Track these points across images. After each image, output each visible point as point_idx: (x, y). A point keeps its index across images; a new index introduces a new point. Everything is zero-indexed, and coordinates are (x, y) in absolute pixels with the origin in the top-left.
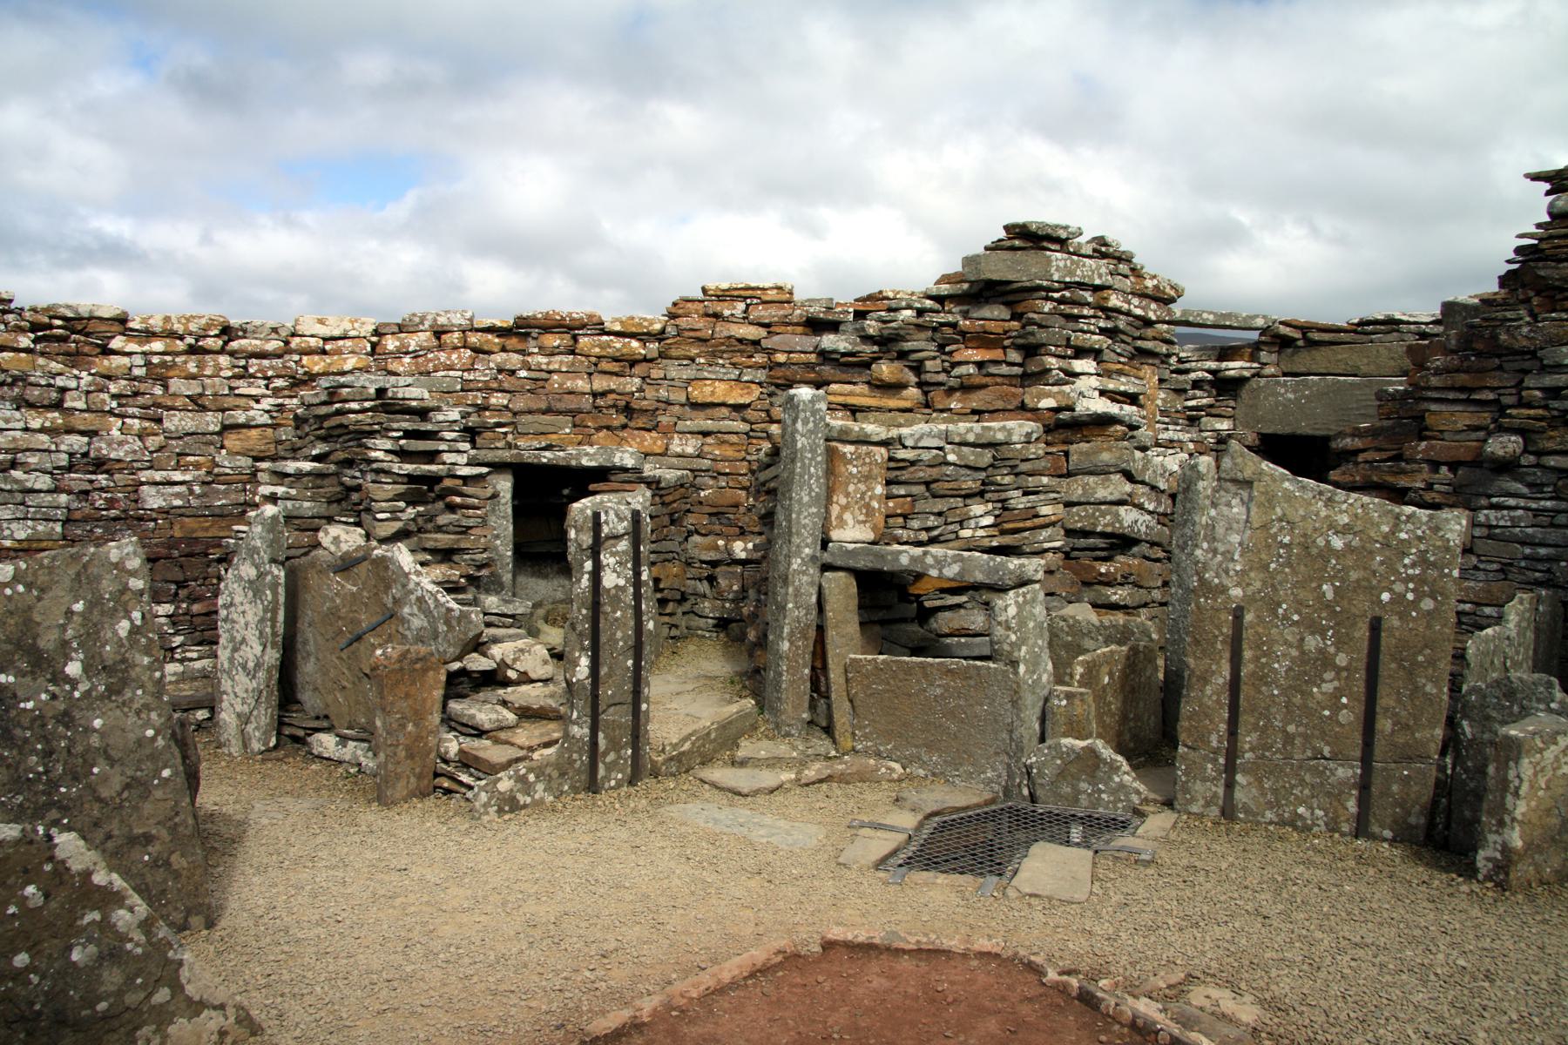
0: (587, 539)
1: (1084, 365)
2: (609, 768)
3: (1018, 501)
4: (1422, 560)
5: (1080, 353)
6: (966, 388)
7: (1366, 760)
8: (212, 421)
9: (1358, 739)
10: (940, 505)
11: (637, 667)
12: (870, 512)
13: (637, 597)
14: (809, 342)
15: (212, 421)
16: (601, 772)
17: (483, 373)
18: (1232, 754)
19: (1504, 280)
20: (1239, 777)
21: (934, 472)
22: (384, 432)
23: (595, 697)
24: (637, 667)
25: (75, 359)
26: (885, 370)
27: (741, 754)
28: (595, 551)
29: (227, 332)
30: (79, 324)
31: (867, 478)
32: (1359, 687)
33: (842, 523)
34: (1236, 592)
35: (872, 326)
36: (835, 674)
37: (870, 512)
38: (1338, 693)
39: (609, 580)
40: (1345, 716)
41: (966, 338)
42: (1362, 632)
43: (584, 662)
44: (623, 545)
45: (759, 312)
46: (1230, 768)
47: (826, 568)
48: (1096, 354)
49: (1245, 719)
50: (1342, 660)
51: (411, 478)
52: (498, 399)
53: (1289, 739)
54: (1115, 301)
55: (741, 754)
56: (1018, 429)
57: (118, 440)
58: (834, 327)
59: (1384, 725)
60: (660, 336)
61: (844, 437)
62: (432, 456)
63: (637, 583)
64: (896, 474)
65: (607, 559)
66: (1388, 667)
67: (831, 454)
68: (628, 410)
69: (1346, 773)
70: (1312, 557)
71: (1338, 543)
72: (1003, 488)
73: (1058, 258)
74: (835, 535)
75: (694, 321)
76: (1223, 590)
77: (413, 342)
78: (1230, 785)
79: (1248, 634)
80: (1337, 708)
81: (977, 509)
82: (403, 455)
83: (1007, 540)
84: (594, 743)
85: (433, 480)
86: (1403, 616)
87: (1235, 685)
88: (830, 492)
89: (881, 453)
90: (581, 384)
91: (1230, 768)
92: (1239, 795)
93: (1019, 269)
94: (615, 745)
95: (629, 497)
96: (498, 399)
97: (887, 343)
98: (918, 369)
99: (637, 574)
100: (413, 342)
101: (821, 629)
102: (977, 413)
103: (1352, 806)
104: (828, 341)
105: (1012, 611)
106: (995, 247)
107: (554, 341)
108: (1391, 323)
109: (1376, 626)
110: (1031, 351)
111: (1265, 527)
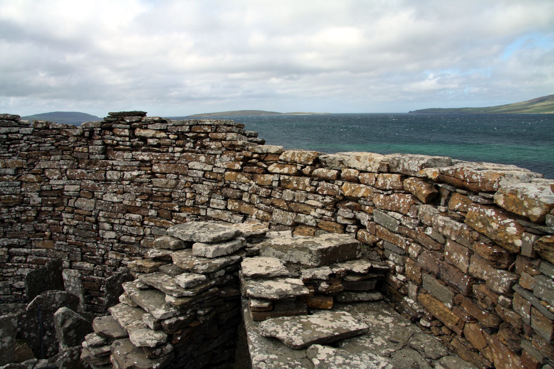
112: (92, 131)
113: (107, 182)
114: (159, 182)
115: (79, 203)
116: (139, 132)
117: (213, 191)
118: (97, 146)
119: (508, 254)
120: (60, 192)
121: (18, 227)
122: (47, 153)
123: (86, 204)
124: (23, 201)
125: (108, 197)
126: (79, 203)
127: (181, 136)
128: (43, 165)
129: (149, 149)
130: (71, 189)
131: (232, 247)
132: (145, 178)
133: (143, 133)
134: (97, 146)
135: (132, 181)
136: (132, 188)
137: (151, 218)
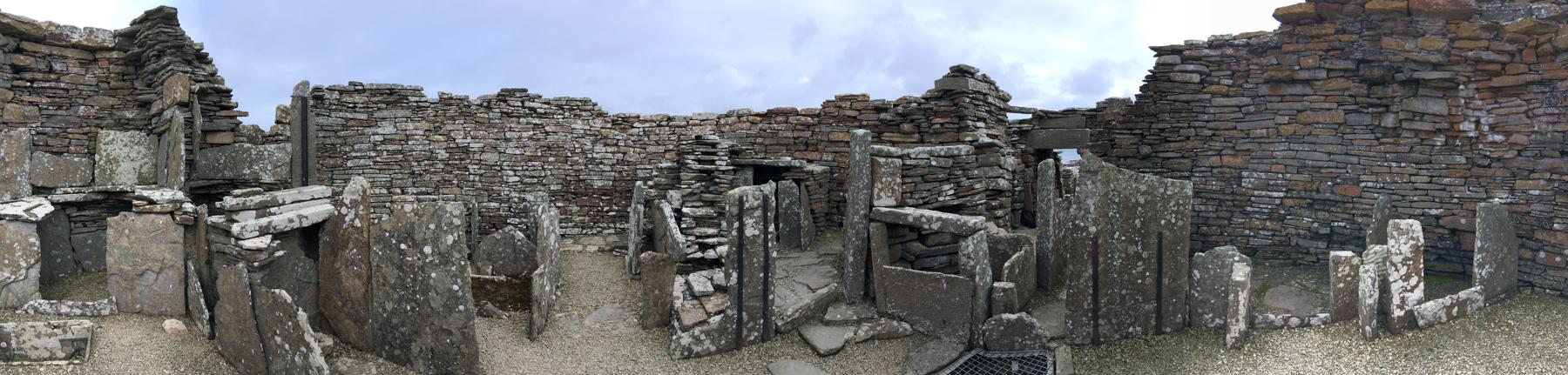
0: (735, 210)
1: (980, 124)
2: (750, 330)
3: (965, 182)
4: (1177, 204)
5: (979, 119)
6: (936, 133)
7: (1159, 299)
8: (661, 149)
9: (1154, 289)
10: (929, 186)
11: (766, 277)
12: (893, 191)
13: (766, 241)
14: (875, 117)
15: (661, 149)
16: (745, 332)
17: (754, 131)
18: (1096, 310)
19: (1142, 89)
20: (1101, 321)
21: (926, 171)
22: (693, 153)
23: (740, 293)
24: (766, 277)
25: (623, 130)
26: (906, 127)
27: (827, 317)
28: (740, 217)
29: (669, 119)
30: (626, 119)
31: (893, 175)
32: (1154, 267)
33: (879, 197)
34: (1093, 229)
35: (900, 109)
36: (875, 275)
37: (893, 191)
38: (1145, 270)
39: (749, 232)
40: (1148, 281)
41: (936, 114)
42: (1154, 240)
43: (735, 275)
44: (758, 213)
45: (856, 105)
46: (1096, 317)
47: (872, 220)
48: (984, 120)
49: (1102, 291)
50: (1145, 255)
51: (700, 171)
52: (759, 140)
53: (1123, 297)
54: (990, 100)
55: (827, 317)
56: (964, 148)
57: (633, 155)
58: (885, 110)
59: (1166, 281)
60: (818, 115)
61: (880, 154)
62: (713, 162)
63: (765, 231)
64: (906, 171)
65: (749, 221)
66: (1166, 254)
67: (873, 163)
68: (807, 144)
69: (1150, 306)
70: (1129, 209)
71: (1142, 200)
72: (957, 177)
73: (971, 82)
74: (876, 203)
75: (832, 109)
76: (1085, 228)
77: (730, 120)
78: (1096, 326)
79: (1101, 250)
80: (1144, 278)
81: (946, 187)
82: (699, 161)
83: (961, 201)
84: (740, 318)
85: (709, 172)
86: (1171, 230)
87: (1095, 277)
88: (873, 182)
89: (898, 162)
90: (789, 134)
91: (1096, 317)
92: (1100, 330)
93: (956, 85)
94: (752, 318)
95: (762, 187)
96: (759, 140)
97: (905, 116)
98: (918, 126)
99: (766, 228)
100: (730, 120)
101: (869, 250)
102: (942, 143)
103: (1153, 322)
104: (883, 116)
105: (971, 248)
106: (947, 76)
107: (779, 119)
108: (1073, 111)
109: (1160, 234)
110: (962, 118)
111: (1107, 194)
112: (489, 102)
113: (507, 140)
114: (551, 138)
115: (484, 156)
116: (527, 104)
117: (594, 143)
118: (495, 114)
119: (296, 243)
120: (466, 150)
121: (427, 178)
122: (453, 118)
123: (491, 157)
124: (432, 157)
125: (509, 151)
126: (484, 156)
127: (561, 107)
128: (449, 127)
129: (540, 116)
130: (476, 146)
131: (1236, 312)
132: (541, 136)
133: (532, 104)
134: (495, 114)
135: (530, 138)
136: (531, 143)
137: (550, 163)
